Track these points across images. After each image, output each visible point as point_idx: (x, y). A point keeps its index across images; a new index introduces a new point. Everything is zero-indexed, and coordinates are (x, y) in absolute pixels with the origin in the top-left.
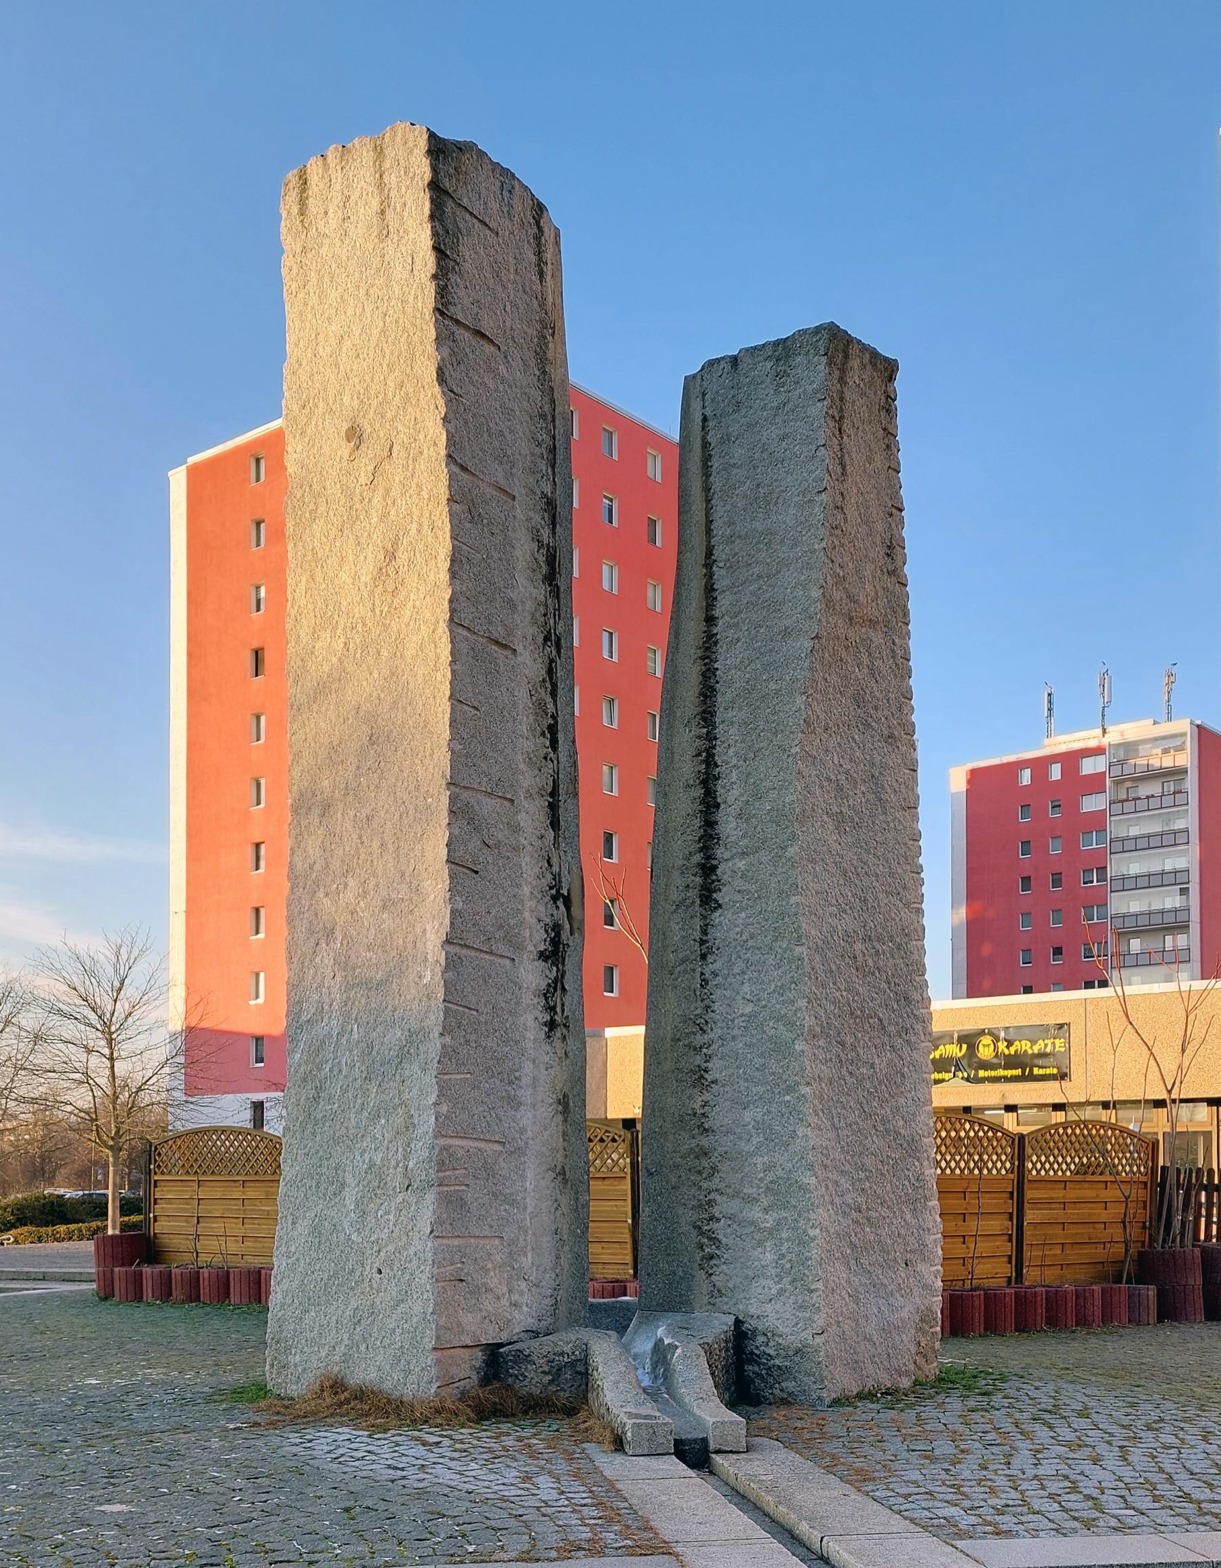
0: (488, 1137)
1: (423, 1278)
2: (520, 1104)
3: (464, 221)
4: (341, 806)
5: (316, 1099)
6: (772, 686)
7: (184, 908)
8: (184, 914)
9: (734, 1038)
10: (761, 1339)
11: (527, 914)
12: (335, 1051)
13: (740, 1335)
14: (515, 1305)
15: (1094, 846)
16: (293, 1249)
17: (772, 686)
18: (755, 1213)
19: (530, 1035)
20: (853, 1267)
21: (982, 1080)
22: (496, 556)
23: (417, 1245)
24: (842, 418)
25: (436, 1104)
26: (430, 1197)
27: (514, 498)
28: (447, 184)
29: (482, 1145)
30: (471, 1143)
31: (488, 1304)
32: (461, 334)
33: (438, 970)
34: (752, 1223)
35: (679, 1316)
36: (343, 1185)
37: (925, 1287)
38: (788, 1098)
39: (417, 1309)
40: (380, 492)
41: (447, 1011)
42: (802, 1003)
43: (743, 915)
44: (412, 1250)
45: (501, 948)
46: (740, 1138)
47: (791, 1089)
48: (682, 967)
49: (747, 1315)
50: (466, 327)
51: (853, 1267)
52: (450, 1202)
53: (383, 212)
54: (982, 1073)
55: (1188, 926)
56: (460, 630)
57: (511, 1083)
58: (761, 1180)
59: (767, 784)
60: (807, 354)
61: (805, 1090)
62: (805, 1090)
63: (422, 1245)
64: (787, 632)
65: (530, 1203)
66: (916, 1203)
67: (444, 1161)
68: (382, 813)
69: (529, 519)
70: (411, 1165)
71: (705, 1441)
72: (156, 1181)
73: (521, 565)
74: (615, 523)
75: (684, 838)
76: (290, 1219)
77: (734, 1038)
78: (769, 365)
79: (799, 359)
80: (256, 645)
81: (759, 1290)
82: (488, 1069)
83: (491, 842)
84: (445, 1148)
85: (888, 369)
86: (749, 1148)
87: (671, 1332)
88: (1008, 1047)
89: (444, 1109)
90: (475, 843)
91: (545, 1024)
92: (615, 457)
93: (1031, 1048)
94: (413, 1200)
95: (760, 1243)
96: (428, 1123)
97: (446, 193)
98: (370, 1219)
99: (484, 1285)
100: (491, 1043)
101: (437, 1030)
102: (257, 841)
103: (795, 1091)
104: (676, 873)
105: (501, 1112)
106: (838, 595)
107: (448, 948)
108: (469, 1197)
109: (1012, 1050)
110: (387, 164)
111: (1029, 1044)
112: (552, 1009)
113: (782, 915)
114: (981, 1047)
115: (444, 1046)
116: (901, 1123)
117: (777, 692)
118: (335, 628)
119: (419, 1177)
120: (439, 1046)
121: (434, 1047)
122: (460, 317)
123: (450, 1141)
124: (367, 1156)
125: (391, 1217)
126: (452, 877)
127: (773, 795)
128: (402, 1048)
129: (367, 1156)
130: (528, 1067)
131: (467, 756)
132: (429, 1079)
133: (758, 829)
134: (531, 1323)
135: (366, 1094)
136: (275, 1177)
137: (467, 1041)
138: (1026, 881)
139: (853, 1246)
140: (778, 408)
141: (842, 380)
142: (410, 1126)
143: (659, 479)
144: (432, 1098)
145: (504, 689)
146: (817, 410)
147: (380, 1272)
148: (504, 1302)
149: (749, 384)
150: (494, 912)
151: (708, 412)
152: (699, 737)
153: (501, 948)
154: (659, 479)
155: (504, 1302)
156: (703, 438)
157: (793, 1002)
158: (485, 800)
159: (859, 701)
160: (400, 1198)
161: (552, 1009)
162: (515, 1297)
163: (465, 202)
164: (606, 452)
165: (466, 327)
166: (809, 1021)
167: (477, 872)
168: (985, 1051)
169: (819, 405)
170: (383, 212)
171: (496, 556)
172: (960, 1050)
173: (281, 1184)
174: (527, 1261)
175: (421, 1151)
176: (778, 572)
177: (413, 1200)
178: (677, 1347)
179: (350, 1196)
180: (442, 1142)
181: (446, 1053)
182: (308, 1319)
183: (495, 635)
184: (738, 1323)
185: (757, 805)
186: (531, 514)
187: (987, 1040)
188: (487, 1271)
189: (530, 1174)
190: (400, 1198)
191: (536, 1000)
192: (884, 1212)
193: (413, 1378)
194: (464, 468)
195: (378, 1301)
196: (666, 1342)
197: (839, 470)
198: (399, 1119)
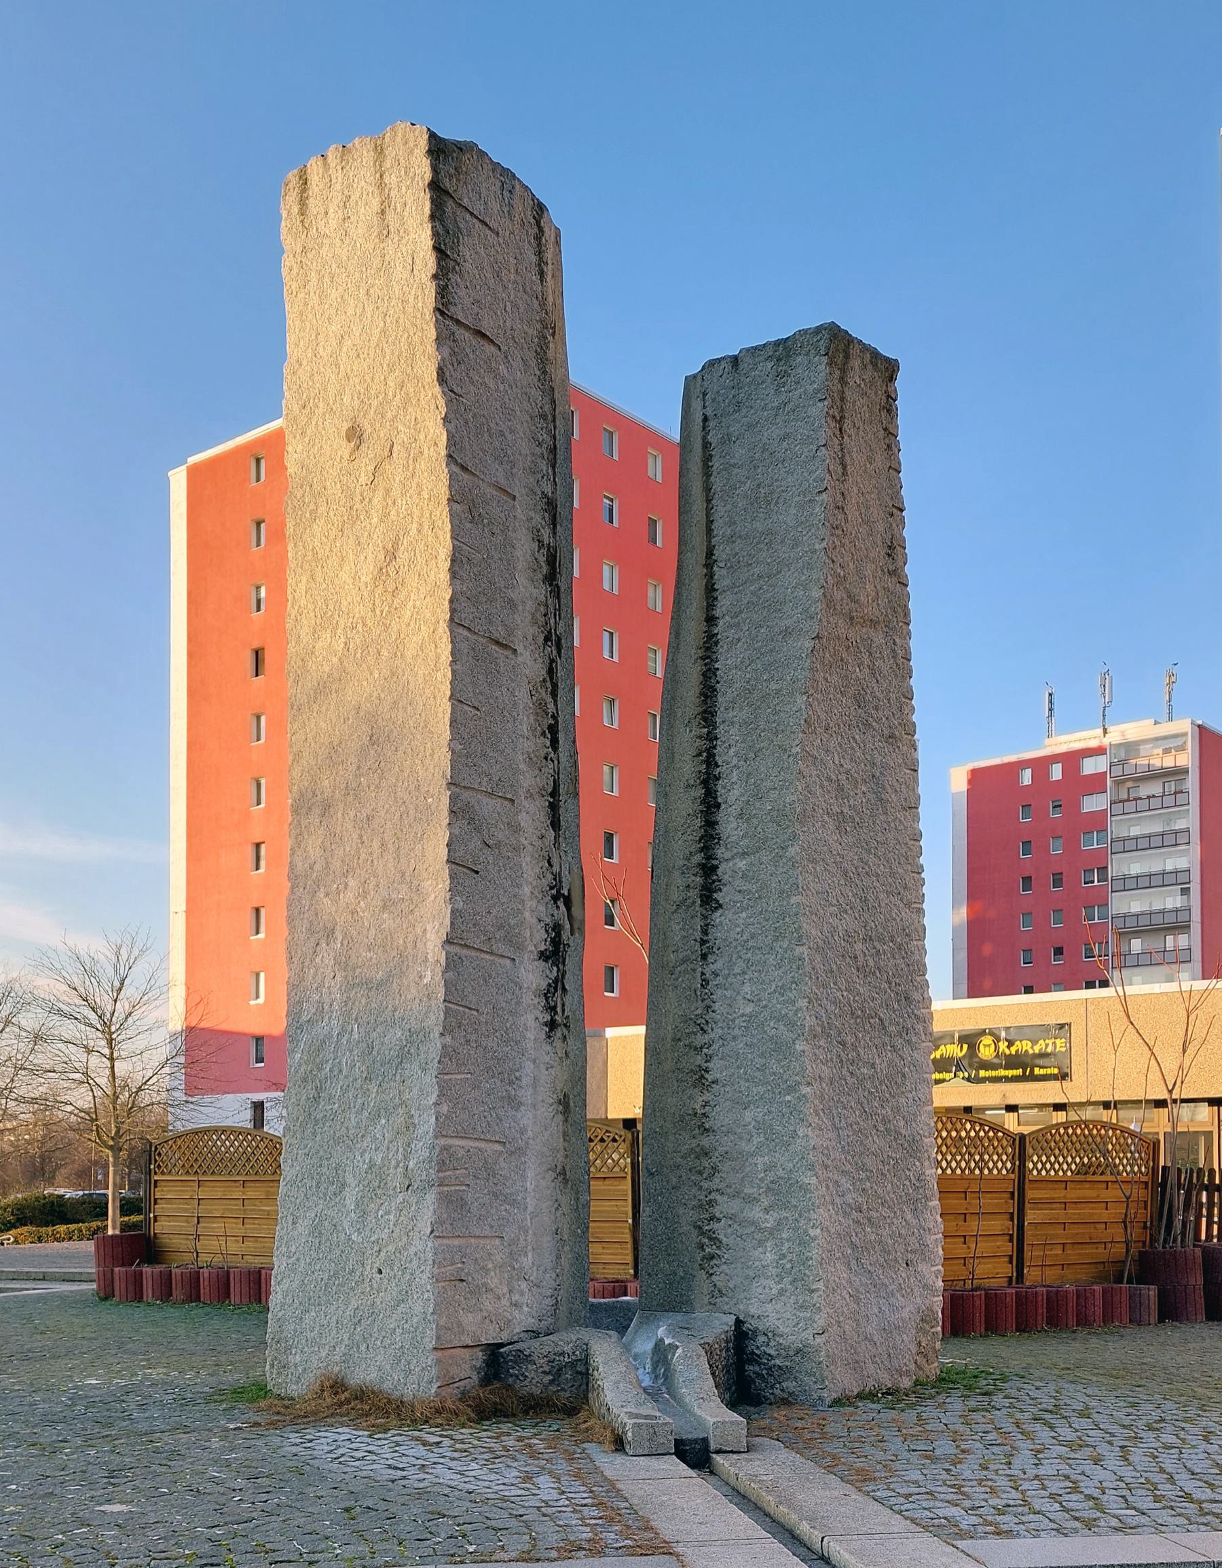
0: (488, 1137)
1: (424, 1278)
2: (520, 1104)
3: (465, 221)
4: (341, 806)
5: (316, 1099)
6: (773, 686)
7: (184, 908)
8: (184, 914)
9: (734, 1038)
10: (762, 1339)
11: (527, 914)
12: (336, 1051)
13: (741, 1335)
14: (516, 1305)
15: (1095, 846)
16: (293, 1249)
17: (773, 686)
18: (756, 1213)
19: (530, 1035)
20: (854, 1267)
21: (983, 1080)
22: (496, 556)
23: (417, 1245)
24: (842, 418)
25: (436, 1104)
26: (431, 1197)
27: (514, 498)
28: (447, 184)
29: (482, 1145)
30: (471, 1143)
31: (488, 1304)
32: (461, 334)
33: (439, 970)
34: (753, 1223)
35: (679, 1316)
36: (343, 1185)
37: (926, 1287)
38: (788, 1098)
39: (418, 1309)
40: (380, 492)
41: (447, 1011)
42: (803, 1003)
43: (744, 915)
44: (412, 1250)
45: (502, 948)
47: (791, 1089)
48: (683, 967)
49: (747, 1315)
50: (467, 327)
51: (854, 1267)
52: (450, 1202)
53: (383, 212)
54: (982, 1073)
55: (1189, 926)
56: (461, 630)
57: (511, 1083)
58: (762, 1180)
59: (768, 784)
60: (808, 354)
61: (806, 1090)
62: (806, 1090)
63: (422, 1245)
64: (787, 632)
65: (531, 1203)
66: (916, 1203)
67: (444, 1161)
68: (382, 813)
69: (529, 519)
70: (411, 1165)
71: (705, 1441)
72: (156, 1181)
73: (521, 565)
74: (616, 523)
75: (684, 838)
76: (290, 1219)
77: (734, 1038)
78: (769, 365)
79: (799, 359)
80: (256, 645)
81: (760, 1290)
82: (488, 1069)
83: (491, 842)
84: (446, 1148)
85: (888, 369)
86: (749, 1148)
87: (671, 1332)
88: (1008, 1047)
89: (445, 1109)
90: (476, 843)
91: (546, 1024)
92: (616, 457)
93: (1032, 1048)
94: (413, 1200)
95: (761, 1243)
96: (428, 1123)
97: (447, 193)
98: (371, 1219)
99: (485, 1285)
100: (491, 1043)
101: (438, 1030)
102: (258, 841)
103: (796, 1091)
104: (677, 873)
105: (501, 1112)
106: (838, 595)
107: (448, 948)
108: (469, 1197)
109: (1013, 1050)
110: (388, 164)
111: (1030, 1044)
112: (553, 1009)
113: (783, 915)
114: (981, 1047)
115: (444, 1046)
116: (902, 1123)
117: (778, 692)
118: (335, 628)
119: (420, 1177)
120: (439, 1046)
121: (434, 1047)
122: (460, 317)
123: (450, 1141)
124: (367, 1156)
125: (391, 1217)
126: (452, 877)
127: (774, 795)
128: (402, 1048)
129: (367, 1156)
130: (529, 1067)
131: (468, 756)
132: (430, 1079)
133: (759, 829)
134: (531, 1323)
135: (366, 1094)
136: (275, 1177)
137: (468, 1041)
138: (1027, 881)
139: (854, 1246)
140: (779, 408)
141: (843, 380)
142: (410, 1126)
143: (659, 479)
144: (433, 1098)
145: (504, 689)
146: (818, 410)
147: (380, 1272)
148: (505, 1302)
149: (750, 384)
150: (494, 912)
151: (709, 412)
152: (700, 737)
153: (502, 948)
154: (659, 479)
155: (505, 1302)
156: (704, 438)
157: (793, 1002)
158: (485, 800)
159: (859, 701)
160: (400, 1198)
161: (553, 1009)
162: (516, 1297)
163: (465, 202)
164: (606, 452)
165: (467, 327)
166: (810, 1021)
167: (477, 872)
168: (986, 1051)
169: (820, 405)
170: (383, 212)
171: (496, 556)
172: (961, 1050)
173: (282, 1184)
174: (527, 1261)
175: (422, 1151)
176: (779, 572)
177: (413, 1200)
178: (677, 1347)
179: (350, 1196)
180: (442, 1142)
181: (447, 1053)
182: (308, 1319)
183: (496, 635)
184: (739, 1323)
185: (758, 805)
186: (532, 514)
187: (987, 1040)
188: (487, 1271)
189: (530, 1174)
190: (400, 1198)
191: (536, 1000)
192: (885, 1212)
193: (413, 1378)
194: (464, 468)
195: (378, 1301)
196: (667, 1342)
197: (840, 470)
198: (399, 1119)
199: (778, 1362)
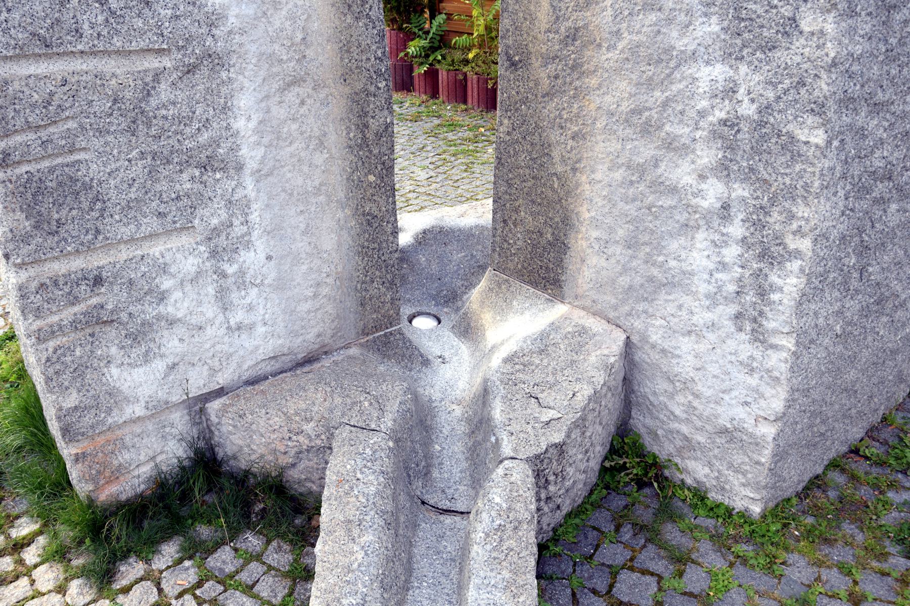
34: (673, 190)
46: (670, 21)
58: (702, 114)
86: (682, 43)
189: (245, 101)
199: (685, 429)
